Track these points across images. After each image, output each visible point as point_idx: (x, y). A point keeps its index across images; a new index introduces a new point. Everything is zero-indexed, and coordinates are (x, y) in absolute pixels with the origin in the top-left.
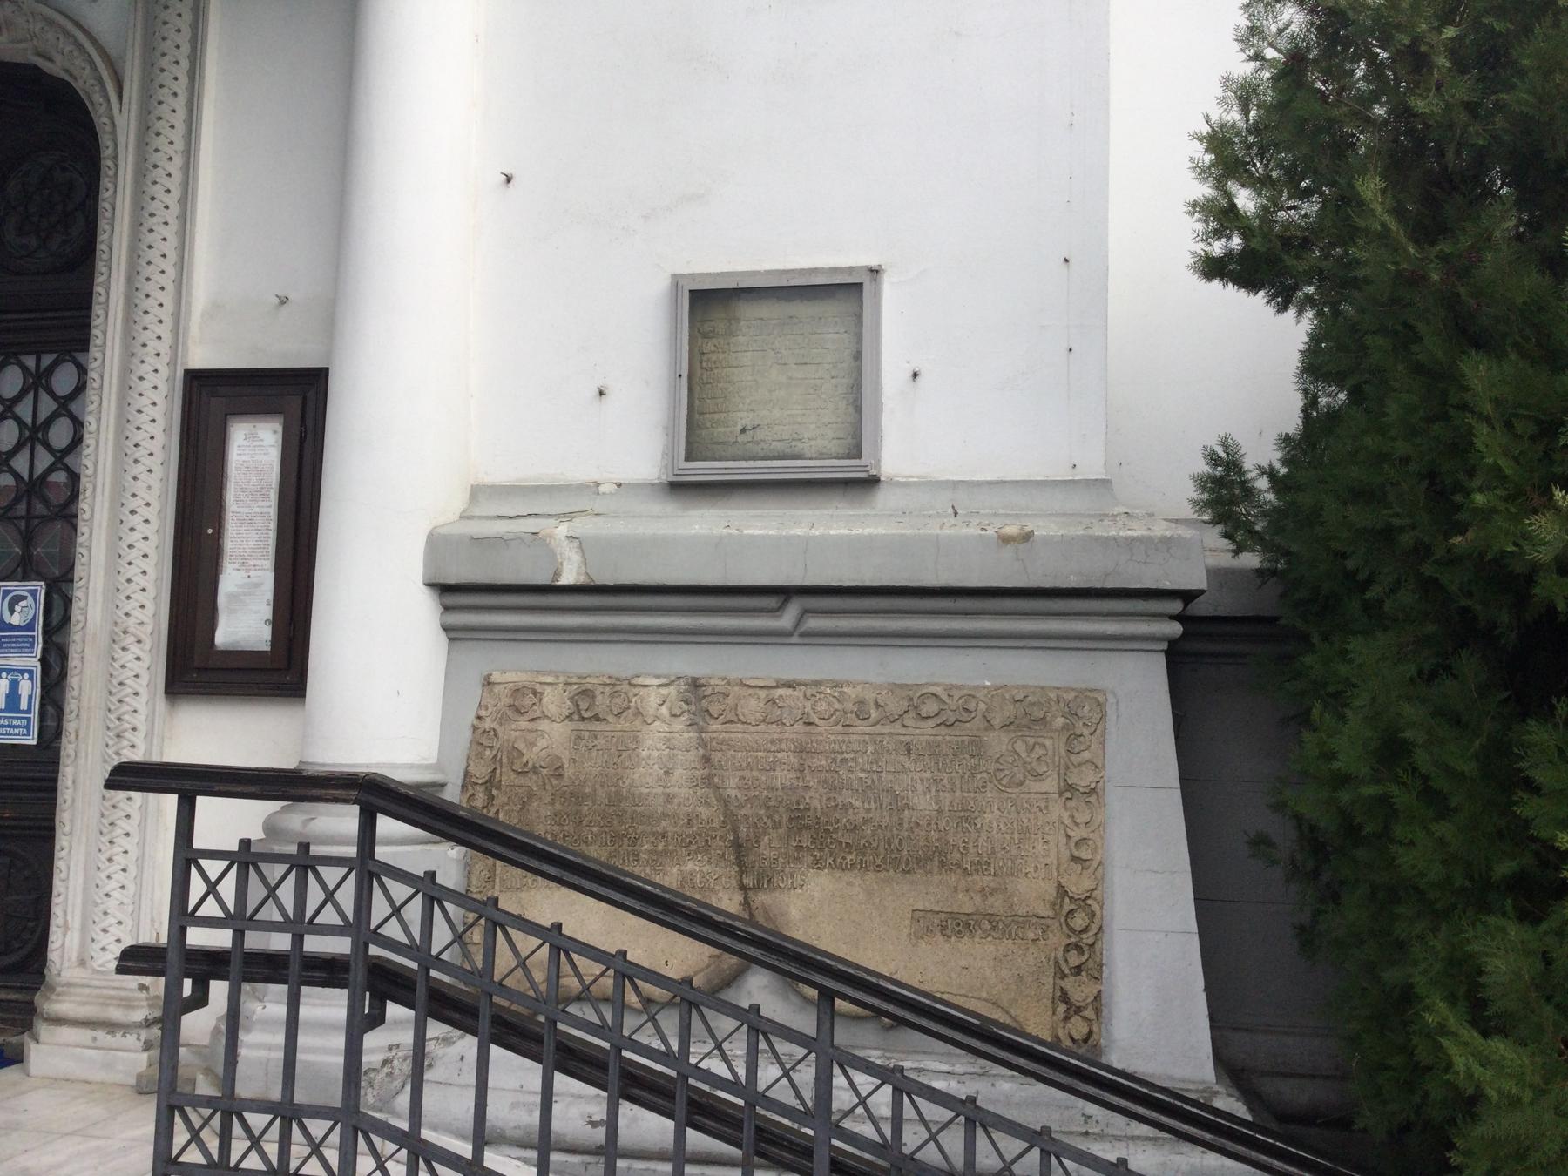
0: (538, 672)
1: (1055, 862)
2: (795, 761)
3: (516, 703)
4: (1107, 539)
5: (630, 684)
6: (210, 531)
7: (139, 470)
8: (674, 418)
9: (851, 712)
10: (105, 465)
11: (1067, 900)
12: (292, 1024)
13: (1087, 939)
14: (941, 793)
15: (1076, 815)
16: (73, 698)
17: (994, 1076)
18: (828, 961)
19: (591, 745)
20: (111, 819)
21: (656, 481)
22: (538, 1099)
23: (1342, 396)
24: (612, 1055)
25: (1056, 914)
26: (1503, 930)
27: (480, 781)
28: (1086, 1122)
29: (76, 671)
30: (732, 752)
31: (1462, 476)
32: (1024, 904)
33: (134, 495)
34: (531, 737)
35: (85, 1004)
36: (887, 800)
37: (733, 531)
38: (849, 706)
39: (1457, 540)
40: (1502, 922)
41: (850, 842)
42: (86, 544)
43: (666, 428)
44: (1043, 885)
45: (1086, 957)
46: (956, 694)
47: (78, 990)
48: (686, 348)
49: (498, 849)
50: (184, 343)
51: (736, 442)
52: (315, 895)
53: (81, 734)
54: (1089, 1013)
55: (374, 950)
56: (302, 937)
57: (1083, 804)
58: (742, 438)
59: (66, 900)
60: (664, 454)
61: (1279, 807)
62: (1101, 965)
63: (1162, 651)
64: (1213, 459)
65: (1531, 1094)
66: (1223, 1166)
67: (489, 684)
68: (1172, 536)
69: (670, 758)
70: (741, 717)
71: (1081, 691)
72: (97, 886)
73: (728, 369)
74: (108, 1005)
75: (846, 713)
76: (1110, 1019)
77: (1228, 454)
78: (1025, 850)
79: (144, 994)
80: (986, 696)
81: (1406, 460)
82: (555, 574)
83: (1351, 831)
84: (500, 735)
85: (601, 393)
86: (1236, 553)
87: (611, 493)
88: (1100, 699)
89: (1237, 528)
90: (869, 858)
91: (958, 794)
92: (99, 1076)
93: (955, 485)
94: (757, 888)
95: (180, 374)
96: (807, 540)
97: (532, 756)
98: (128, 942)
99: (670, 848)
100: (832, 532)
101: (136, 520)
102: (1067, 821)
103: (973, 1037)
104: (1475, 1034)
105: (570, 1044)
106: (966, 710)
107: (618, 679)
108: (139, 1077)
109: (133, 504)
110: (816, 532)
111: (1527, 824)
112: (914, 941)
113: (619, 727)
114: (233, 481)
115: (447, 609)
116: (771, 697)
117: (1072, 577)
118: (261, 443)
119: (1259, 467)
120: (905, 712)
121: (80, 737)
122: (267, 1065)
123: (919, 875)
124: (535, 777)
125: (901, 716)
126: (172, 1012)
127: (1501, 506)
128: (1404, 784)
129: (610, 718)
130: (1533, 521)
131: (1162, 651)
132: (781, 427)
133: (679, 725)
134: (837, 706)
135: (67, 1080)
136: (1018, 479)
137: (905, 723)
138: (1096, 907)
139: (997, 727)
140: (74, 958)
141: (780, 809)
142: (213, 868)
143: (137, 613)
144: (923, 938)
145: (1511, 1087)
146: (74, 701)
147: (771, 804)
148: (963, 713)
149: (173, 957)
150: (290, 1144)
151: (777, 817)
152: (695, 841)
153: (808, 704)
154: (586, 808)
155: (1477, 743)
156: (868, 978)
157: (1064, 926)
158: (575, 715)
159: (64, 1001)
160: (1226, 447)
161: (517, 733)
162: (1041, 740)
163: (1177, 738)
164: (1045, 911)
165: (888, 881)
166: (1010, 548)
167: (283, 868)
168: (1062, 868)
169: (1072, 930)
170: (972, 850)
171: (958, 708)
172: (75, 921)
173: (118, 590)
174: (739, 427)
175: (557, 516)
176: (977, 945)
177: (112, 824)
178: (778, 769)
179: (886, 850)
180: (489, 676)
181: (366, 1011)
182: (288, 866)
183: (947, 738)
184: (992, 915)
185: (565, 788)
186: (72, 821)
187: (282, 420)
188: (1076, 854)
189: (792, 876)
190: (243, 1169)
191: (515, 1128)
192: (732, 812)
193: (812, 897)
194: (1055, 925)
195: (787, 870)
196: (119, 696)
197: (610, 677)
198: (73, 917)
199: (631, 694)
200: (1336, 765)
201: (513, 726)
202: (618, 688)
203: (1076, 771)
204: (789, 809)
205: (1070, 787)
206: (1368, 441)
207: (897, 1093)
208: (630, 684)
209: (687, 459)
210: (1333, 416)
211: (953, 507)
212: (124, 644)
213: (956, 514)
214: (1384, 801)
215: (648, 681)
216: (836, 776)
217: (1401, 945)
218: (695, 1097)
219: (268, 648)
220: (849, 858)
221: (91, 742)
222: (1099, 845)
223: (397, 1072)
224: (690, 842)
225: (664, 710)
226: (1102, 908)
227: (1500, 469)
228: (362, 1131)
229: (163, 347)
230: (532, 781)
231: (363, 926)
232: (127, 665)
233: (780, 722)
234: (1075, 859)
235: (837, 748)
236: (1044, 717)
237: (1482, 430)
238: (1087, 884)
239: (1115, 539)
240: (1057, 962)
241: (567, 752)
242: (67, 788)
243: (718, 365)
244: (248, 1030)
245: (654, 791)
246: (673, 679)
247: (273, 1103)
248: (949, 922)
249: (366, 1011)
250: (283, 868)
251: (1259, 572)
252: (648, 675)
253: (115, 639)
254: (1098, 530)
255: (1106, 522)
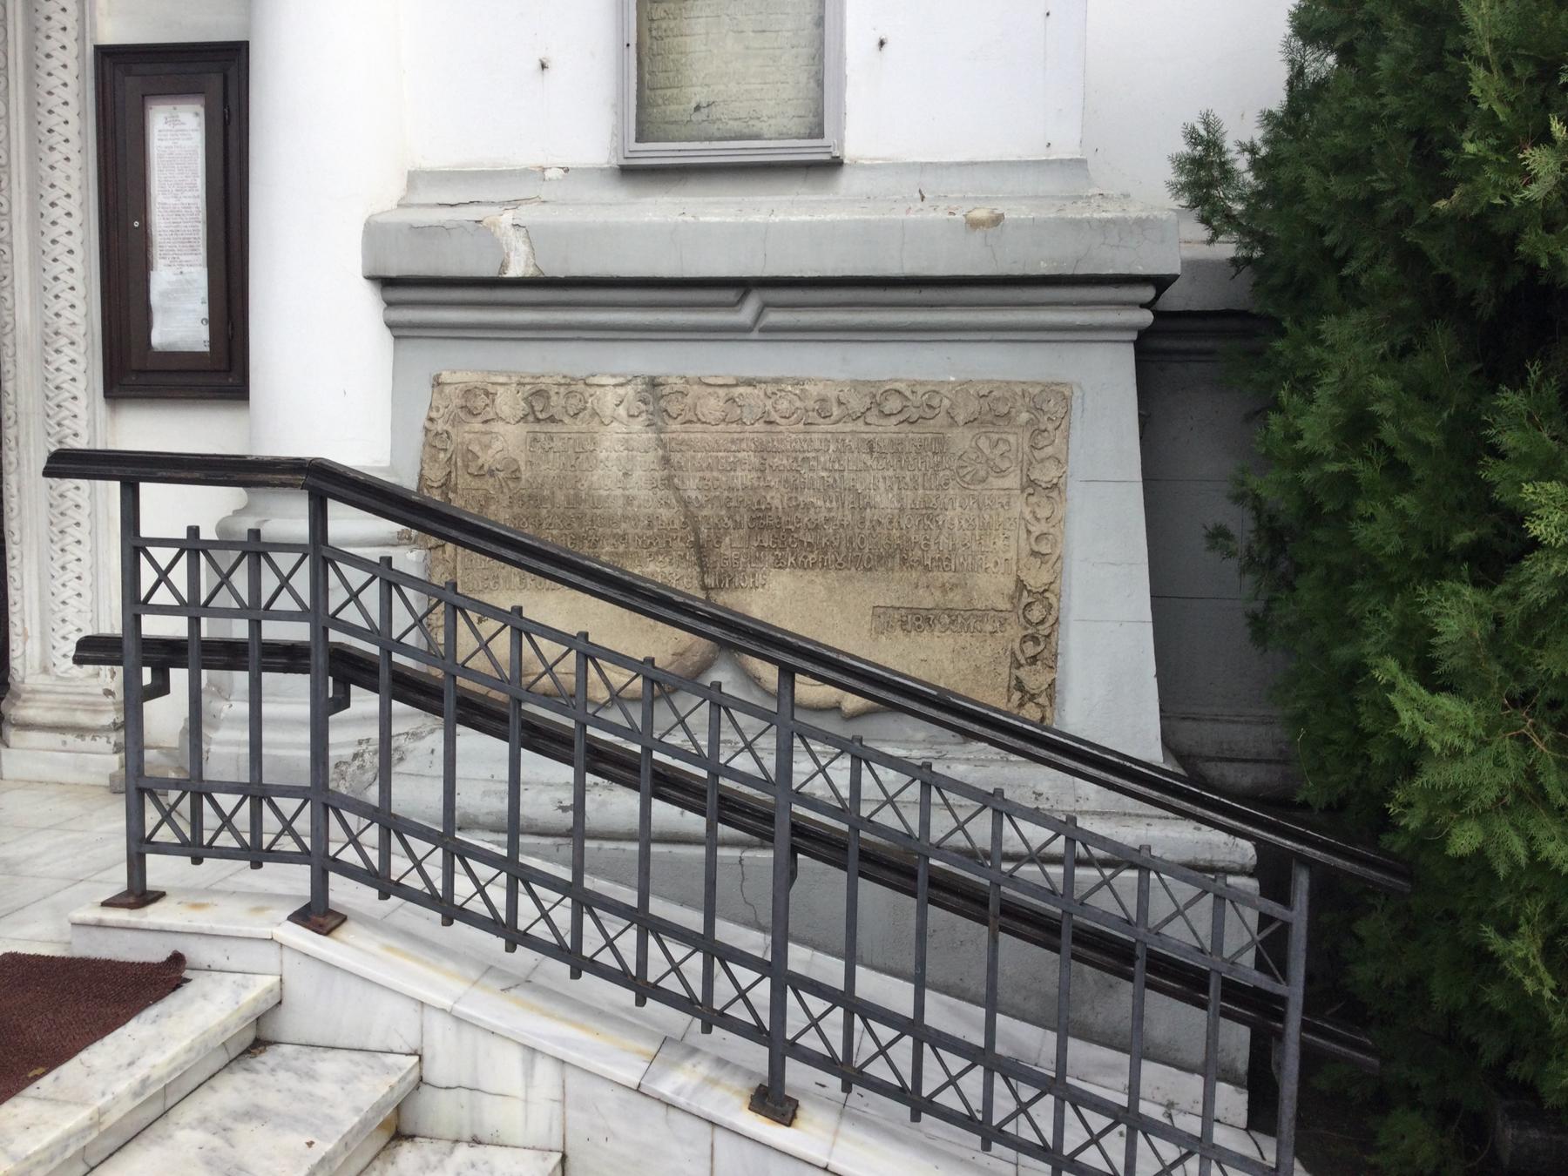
0: (489, 372)
1: (1015, 557)
2: (756, 461)
3: (468, 405)
4: (1080, 221)
5: (586, 384)
6: (136, 224)
7: (56, 157)
8: (622, 95)
9: (813, 410)
10: (18, 152)
11: (1025, 593)
12: (256, 721)
13: (1044, 630)
14: (903, 491)
15: (1037, 510)
16: (9, 403)
17: (950, 759)
18: (789, 639)
19: (547, 447)
20: (61, 527)
21: (606, 166)
22: (506, 787)
23: (1331, 60)
24: (577, 734)
25: (1014, 607)
26: (1457, 593)
27: (435, 485)
28: (1036, 799)
29: (10, 376)
30: (692, 453)
31: (1453, 129)
32: (983, 598)
33: (52, 186)
34: (485, 439)
35: (52, 709)
36: (849, 498)
37: (689, 218)
38: (810, 404)
39: (1442, 204)
40: (1457, 586)
41: (811, 540)
42: (7, 239)
43: (614, 106)
44: (1002, 579)
45: (1042, 647)
46: (920, 390)
47: (43, 696)
48: (633, 14)
49: (454, 533)
50: (92, 16)
51: (691, 121)
52: (269, 583)
53: (22, 440)
54: (1042, 700)
55: (335, 636)
56: (259, 622)
57: (1045, 499)
58: (697, 117)
59: (22, 609)
60: (614, 134)
61: (1238, 499)
62: (1056, 655)
63: (1129, 342)
64: (1194, 138)
65: (1473, 745)
66: (1167, 837)
67: (439, 384)
68: (1148, 217)
69: (631, 459)
70: (700, 416)
71: (1047, 385)
72: (53, 594)
73: (680, 38)
74: (76, 710)
75: (807, 411)
76: (1063, 704)
77: (1208, 132)
78: (986, 546)
79: (110, 699)
80: (950, 391)
81: (1393, 118)
82: (502, 265)
83: (1311, 512)
84: (454, 437)
85: (543, 66)
86: (1211, 242)
87: (558, 179)
88: (1066, 393)
89: (1214, 212)
90: (830, 557)
91: (921, 491)
92: (71, 777)
93: (924, 167)
94: (719, 587)
95: (90, 51)
96: (767, 226)
97: (487, 458)
98: (89, 631)
99: (631, 549)
100: (793, 219)
101: (57, 213)
102: (1029, 517)
103: (930, 707)
104: (1423, 691)
105: (536, 723)
106: (930, 407)
107: (573, 379)
108: (112, 777)
109: (53, 195)
110: (776, 219)
111: (1491, 486)
112: (874, 636)
113: (576, 428)
114: (156, 169)
115: (390, 304)
116: (730, 396)
117: (1042, 263)
118: (182, 127)
119: (1241, 144)
120: (868, 409)
121: (20, 444)
122: (237, 761)
123: (880, 572)
124: (491, 480)
125: (863, 413)
126: (135, 699)
127: (1493, 157)
128: (1370, 459)
129: (567, 420)
130: (1528, 156)
131: (1129, 342)
132: (737, 104)
133: (637, 425)
134: (798, 404)
135: (41, 782)
136: (990, 159)
137: (868, 420)
138: (1053, 600)
139: (961, 423)
140: (36, 664)
141: (741, 509)
142: (163, 556)
143: (67, 313)
144: (883, 633)
145: (1453, 738)
146: (11, 407)
147: (732, 504)
148: (927, 410)
149: (129, 646)
150: (261, 834)
151: (738, 518)
152: (659, 543)
153: (769, 403)
154: (545, 511)
155: (1445, 415)
156: (828, 653)
157: (1022, 619)
158: (527, 417)
159: (31, 707)
160: (1207, 124)
161: (471, 436)
162: (1004, 436)
163: (1141, 438)
164: (1004, 605)
165: (850, 579)
166: (979, 234)
167: (235, 554)
168: (1022, 562)
169: (1029, 622)
170: (933, 547)
171: (922, 405)
172: (34, 629)
173: (45, 289)
174: (694, 105)
175: (502, 204)
176: (936, 639)
177: (62, 532)
178: (739, 469)
179: (848, 548)
180: (438, 376)
181: (330, 695)
182: (240, 552)
183: (911, 435)
184: (952, 609)
185: (524, 491)
186: (21, 530)
187: (203, 101)
188: (1036, 548)
189: (754, 576)
190: (216, 847)
191: (488, 814)
192: (692, 513)
193: (774, 596)
194: (1012, 618)
195: (749, 570)
196: (56, 401)
197: (565, 377)
198: (31, 624)
199: (587, 395)
200: (1300, 445)
201: (467, 428)
202: (573, 388)
203: (1040, 465)
204: (750, 509)
205: (1033, 483)
206: (1356, 102)
207: (855, 761)
208: (586, 384)
209: (637, 140)
210: (1321, 85)
211: (920, 191)
212: (56, 346)
213: (923, 198)
214: (1349, 478)
215: (604, 381)
216: (798, 475)
217: (1354, 623)
218: (660, 770)
219: (207, 349)
220: (811, 557)
221: (32, 449)
222: (1059, 539)
223: (368, 765)
224: (651, 543)
225: (622, 411)
226: (1059, 600)
227: (1494, 115)
228: (332, 808)
229: (70, 20)
230: (489, 484)
231: (321, 610)
232: (62, 368)
233: (740, 421)
234: (1034, 554)
235: (798, 447)
236: (1009, 413)
237: (1480, 73)
238: (1045, 577)
239: (1089, 221)
240: (1013, 653)
241: (523, 455)
242: (12, 496)
243: (669, 33)
244: (216, 728)
245: (614, 493)
246: (630, 378)
247: (244, 784)
248: (910, 617)
249: (330, 695)
250: (235, 554)
251: (1234, 261)
252: (603, 374)
253: (48, 338)
254: (1071, 213)
255: (1080, 204)
